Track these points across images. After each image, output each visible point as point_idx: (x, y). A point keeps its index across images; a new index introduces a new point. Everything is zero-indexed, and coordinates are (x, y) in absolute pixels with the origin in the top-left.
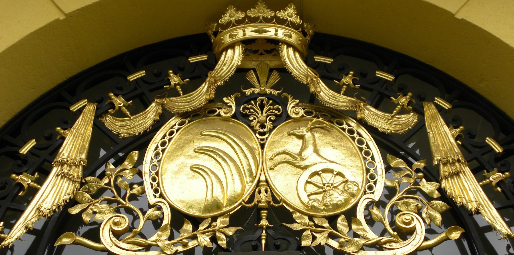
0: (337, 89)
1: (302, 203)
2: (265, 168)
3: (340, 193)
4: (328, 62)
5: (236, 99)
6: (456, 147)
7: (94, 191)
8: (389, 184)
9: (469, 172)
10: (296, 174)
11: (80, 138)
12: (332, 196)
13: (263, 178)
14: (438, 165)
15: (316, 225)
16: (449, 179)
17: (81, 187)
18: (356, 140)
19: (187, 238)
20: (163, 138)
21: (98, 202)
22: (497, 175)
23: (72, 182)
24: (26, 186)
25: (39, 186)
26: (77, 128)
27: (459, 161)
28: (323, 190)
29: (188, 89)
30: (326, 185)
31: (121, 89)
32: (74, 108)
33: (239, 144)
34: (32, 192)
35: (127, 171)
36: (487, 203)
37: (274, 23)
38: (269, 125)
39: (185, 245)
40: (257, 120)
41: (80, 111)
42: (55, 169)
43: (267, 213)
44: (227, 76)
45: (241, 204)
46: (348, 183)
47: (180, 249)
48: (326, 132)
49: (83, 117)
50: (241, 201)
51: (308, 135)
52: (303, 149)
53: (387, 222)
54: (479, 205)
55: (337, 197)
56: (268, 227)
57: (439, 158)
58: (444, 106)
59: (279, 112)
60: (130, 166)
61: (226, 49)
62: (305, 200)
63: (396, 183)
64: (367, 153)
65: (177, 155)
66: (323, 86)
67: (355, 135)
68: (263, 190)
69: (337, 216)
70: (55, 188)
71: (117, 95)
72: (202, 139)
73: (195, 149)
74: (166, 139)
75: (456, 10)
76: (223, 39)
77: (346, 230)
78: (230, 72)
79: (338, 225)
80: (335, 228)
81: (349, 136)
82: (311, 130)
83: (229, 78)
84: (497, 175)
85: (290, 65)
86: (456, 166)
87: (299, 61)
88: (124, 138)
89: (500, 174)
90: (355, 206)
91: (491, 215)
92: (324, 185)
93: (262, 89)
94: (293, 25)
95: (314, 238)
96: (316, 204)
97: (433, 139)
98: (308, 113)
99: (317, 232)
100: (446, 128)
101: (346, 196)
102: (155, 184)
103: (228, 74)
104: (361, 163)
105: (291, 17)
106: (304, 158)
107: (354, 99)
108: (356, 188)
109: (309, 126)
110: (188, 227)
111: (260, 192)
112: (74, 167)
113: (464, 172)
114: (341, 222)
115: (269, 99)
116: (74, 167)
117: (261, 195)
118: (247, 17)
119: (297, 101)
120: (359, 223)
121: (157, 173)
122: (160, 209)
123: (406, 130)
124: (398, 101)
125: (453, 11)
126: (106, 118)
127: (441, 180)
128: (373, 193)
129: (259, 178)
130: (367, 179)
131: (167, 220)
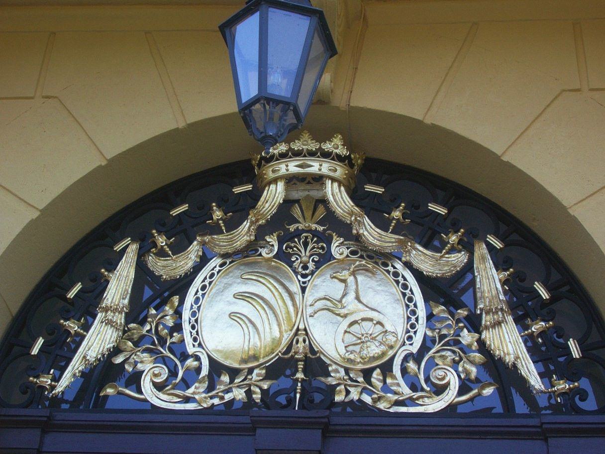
0: (383, 225)
1: (340, 356)
2: (305, 316)
3: (377, 344)
4: (379, 192)
5: (278, 237)
6: (502, 293)
7: (136, 337)
8: (429, 333)
9: (512, 322)
10: (336, 323)
11: (123, 281)
12: (369, 349)
13: (302, 327)
14: (481, 314)
15: (351, 379)
16: (491, 330)
17: (124, 334)
18: (400, 284)
19: (222, 392)
20: (204, 281)
21: (139, 351)
22: (540, 325)
23: (115, 329)
24: (72, 332)
25: (85, 333)
26: (120, 270)
27: (502, 309)
28: (361, 341)
29: (232, 225)
30: (365, 335)
31: (164, 225)
32: (118, 248)
33: (279, 289)
34: (79, 339)
35: (168, 318)
36: (526, 356)
37: (318, 157)
38: (311, 266)
39: (222, 398)
40: (299, 261)
41: (124, 250)
42: (99, 315)
43: (303, 365)
44: (268, 214)
45: (277, 354)
46: (387, 334)
47: (216, 401)
48: (370, 275)
49: (127, 255)
50: (278, 351)
51: (351, 279)
52: (344, 296)
53: (422, 377)
54: (517, 358)
55: (374, 349)
56: (303, 380)
57: (482, 306)
58: (496, 245)
59: (323, 251)
60: (171, 312)
61: (269, 183)
62: (342, 351)
63: (436, 333)
64: (410, 300)
65: (217, 301)
66: (369, 225)
67: (400, 278)
68: (301, 339)
69: (372, 370)
70: (99, 336)
71: (159, 232)
72: (242, 283)
73: (235, 294)
74: (207, 283)
75: (501, 153)
76: (265, 174)
77: (379, 385)
78: (272, 210)
79: (373, 380)
80: (370, 383)
81: (393, 279)
82: (353, 274)
83: (271, 216)
84: (540, 325)
85: (335, 203)
86: (499, 315)
87: (343, 196)
88: (166, 280)
89: (543, 324)
90: (392, 359)
91: (528, 369)
92: (363, 335)
93: (306, 225)
94: (339, 158)
95: (348, 393)
96: (352, 357)
97: (479, 284)
98: (353, 253)
99: (350, 386)
100: (494, 270)
101: (383, 348)
102: (194, 332)
103: (270, 213)
104: (403, 310)
105: (337, 148)
106: (345, 305)
107: (402, 238)
108: (395, 339)
109: (352, 270)
110: (225, 378)
111: (297, 342)
112: (117, 314)
113: (506, 322)
114: (376, 375)
115: (314, 236)
116: (117, 314)
117: (299, 345)
118: (290, 149)
119: (342, 240)
120: (394, 377)
121: (196, 321)
122: (197, 358)
123: (454, 272)
124: (449, 238)
125: (499, 153)
126: (149, 257)
127: (482, 331)
128: (411, 344)
129: (298, 327)
130: (407, 329)
131: (205, 371)
